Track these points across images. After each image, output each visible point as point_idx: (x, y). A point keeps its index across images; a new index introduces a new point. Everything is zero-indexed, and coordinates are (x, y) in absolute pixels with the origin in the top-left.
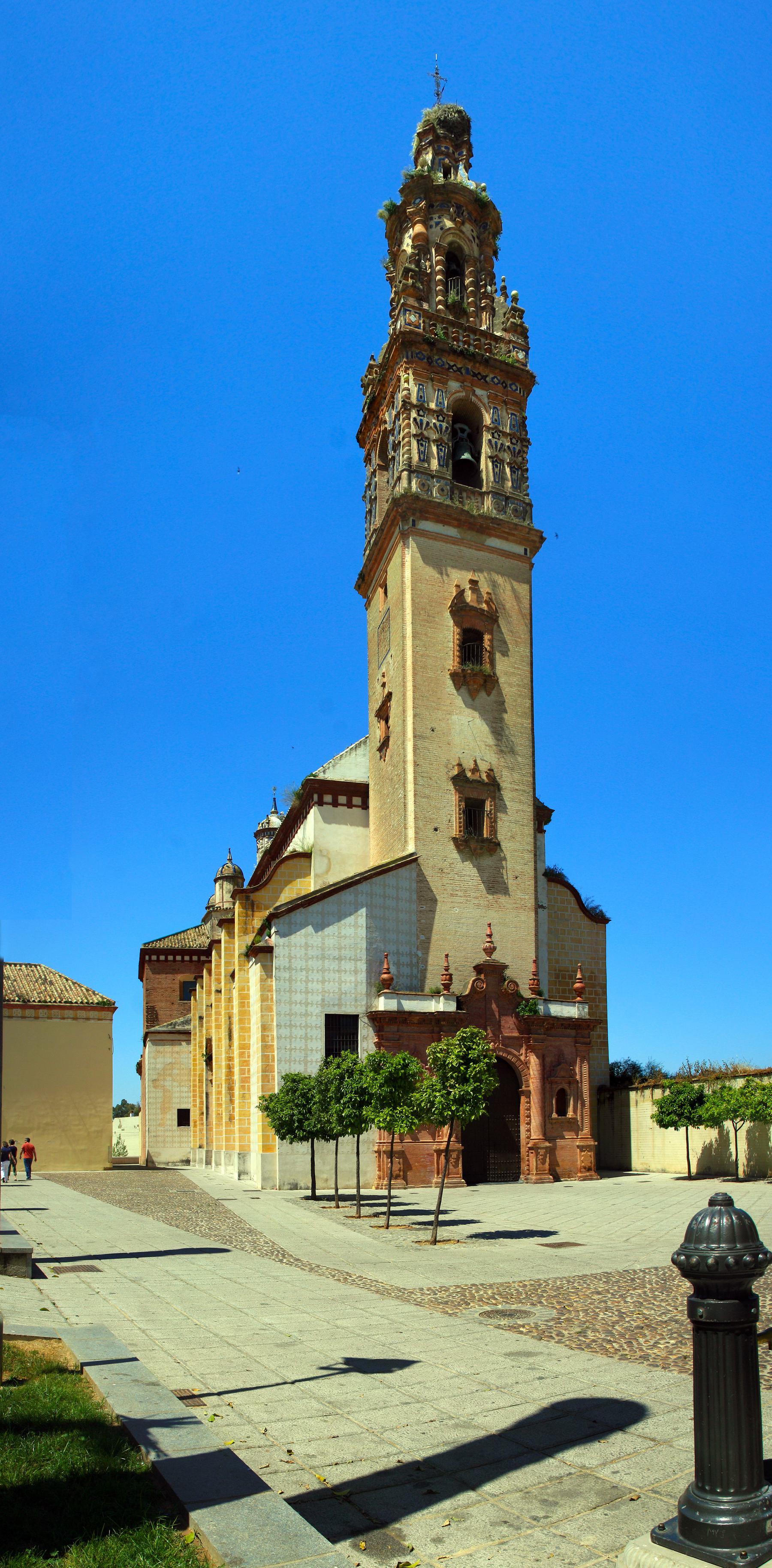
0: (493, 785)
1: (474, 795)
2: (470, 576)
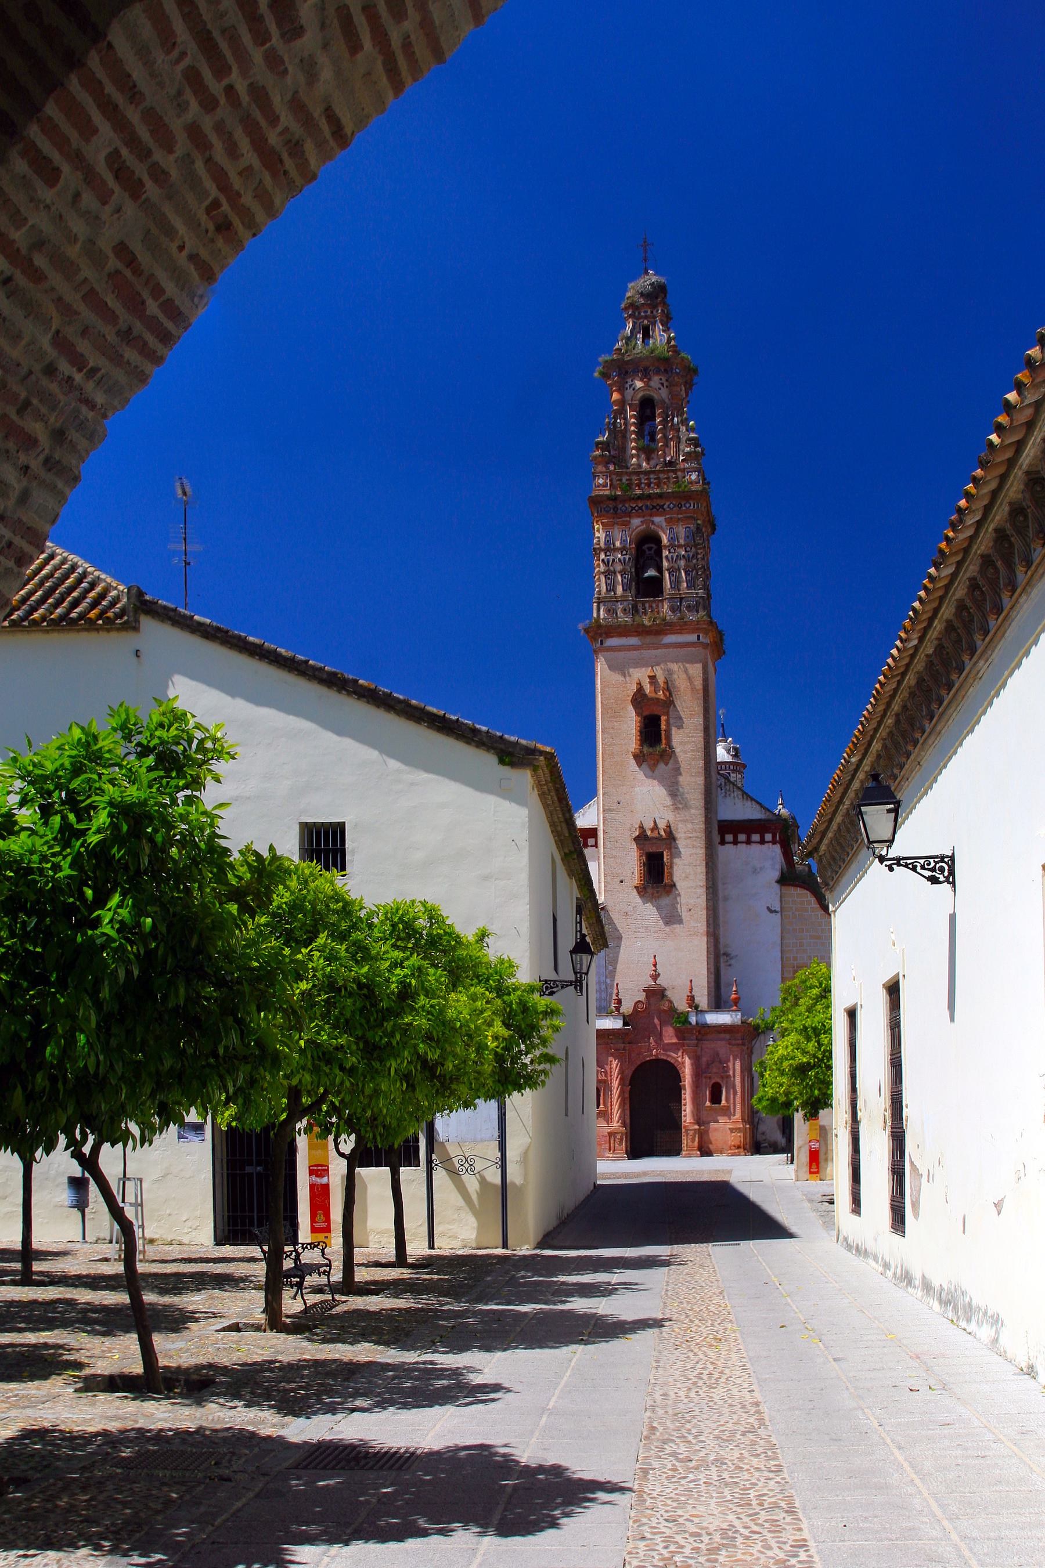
0: (670, 837)
2: (648, 671)
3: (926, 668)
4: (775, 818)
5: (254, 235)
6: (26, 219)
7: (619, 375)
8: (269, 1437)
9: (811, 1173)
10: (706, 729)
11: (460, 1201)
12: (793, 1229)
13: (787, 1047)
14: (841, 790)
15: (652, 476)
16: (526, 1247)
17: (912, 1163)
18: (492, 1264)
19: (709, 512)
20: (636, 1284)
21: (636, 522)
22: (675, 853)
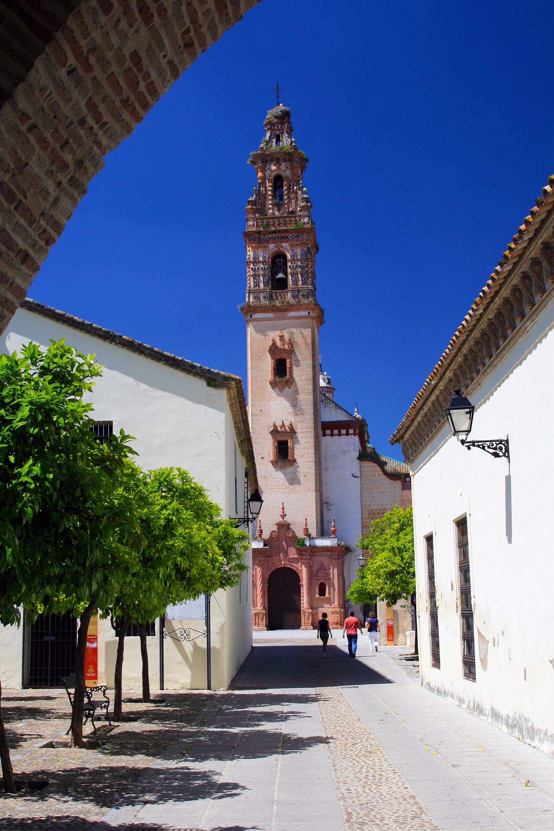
0: (292, 431)
1: (282, 439)
2: (278, 333)
3: (488, 327)
4: (355, 420)
5: (203, 51)
6: (90, 33)
7: (262, 162)
8: (96, 822)
9: (388, 640)
10: (314, 367)
11: (180, 658)
12: (389, 677)
13: (382, 560)
14: (422, 401)
15: (281, 220)
16: (222, 689)
17: (479, 633)
18: (204, 700)
19: (315, 240)
20: (300, 713)
21: (272, 246)
22: (296, 441)
